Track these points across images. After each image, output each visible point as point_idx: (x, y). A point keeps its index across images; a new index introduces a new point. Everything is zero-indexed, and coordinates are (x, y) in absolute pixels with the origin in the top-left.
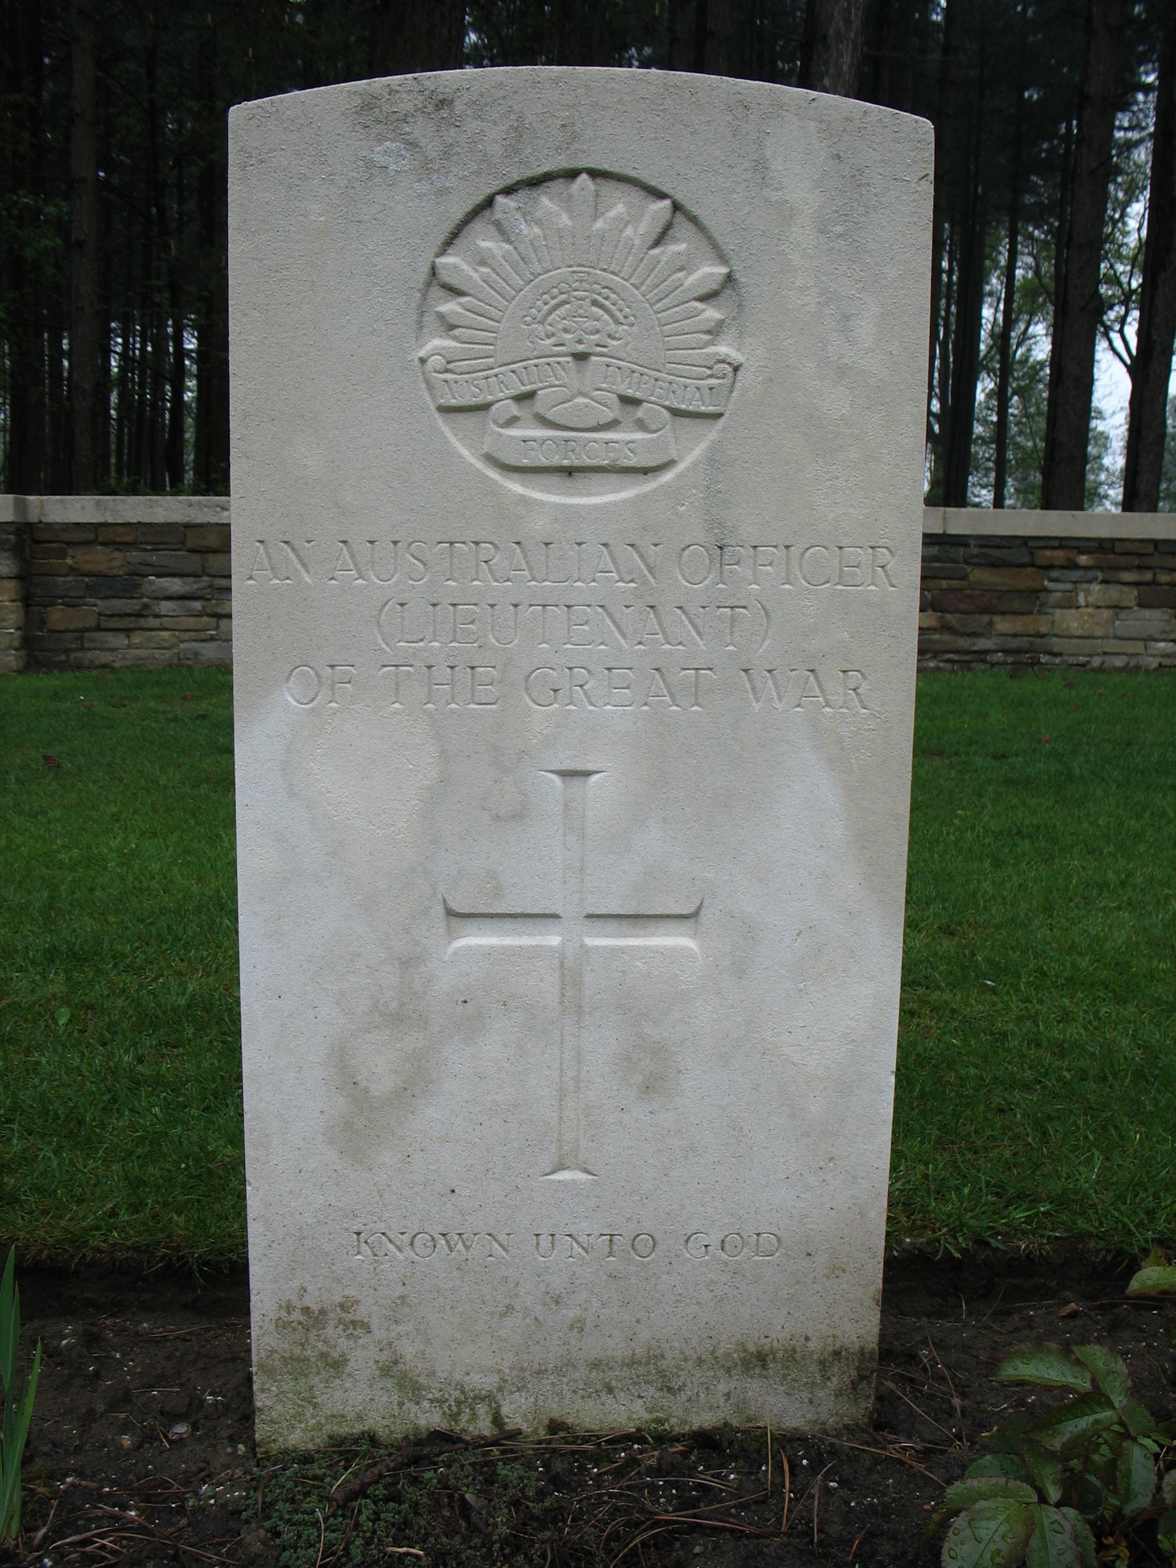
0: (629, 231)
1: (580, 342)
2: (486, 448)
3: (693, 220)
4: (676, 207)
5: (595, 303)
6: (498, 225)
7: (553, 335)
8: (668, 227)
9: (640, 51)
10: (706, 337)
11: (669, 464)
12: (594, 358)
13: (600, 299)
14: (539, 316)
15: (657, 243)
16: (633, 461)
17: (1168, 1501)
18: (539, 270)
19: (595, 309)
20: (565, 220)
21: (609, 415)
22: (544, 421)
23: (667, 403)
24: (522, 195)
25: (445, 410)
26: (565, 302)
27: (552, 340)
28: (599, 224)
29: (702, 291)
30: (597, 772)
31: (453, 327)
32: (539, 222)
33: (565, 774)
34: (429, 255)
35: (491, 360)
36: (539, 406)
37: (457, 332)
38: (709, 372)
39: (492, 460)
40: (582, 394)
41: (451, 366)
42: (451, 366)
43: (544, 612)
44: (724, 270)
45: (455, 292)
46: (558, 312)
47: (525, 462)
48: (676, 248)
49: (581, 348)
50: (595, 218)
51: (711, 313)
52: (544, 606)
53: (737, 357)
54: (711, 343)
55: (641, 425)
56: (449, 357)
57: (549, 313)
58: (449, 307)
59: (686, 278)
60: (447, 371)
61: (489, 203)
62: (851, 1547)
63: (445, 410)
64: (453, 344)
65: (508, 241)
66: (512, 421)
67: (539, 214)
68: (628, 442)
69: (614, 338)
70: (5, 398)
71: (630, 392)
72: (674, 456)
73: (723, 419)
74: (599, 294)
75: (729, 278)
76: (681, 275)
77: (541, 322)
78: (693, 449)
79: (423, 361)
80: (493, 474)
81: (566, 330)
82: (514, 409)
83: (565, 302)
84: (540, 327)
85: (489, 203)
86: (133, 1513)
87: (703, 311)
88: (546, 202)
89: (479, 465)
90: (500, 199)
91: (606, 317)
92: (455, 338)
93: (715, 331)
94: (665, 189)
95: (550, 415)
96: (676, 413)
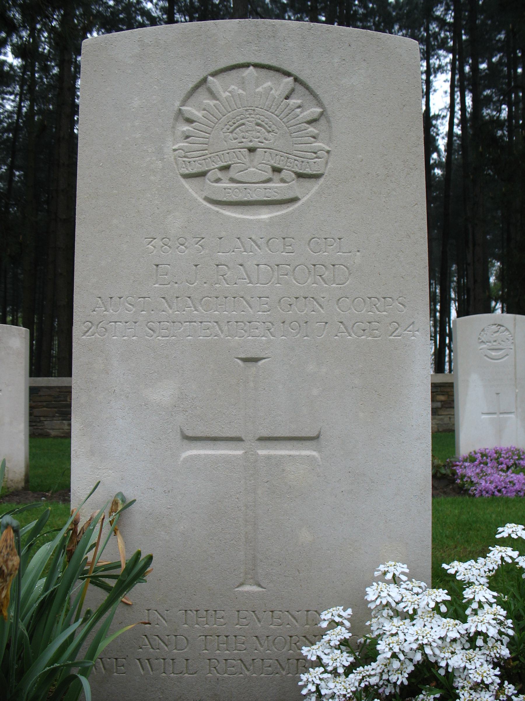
0: (273, 92)
1: (251, 141)
2: (205, 194)
4: (296, 80)
5: (258, 125)
7: (237, 139)
8: (293, 90)
12: (258, 149)
13: (259, 121)
15: (287, 98)
17: (302, 675)
18: (230, 110)
22: (232, 180)
23: (293, 169)
25: (186, 176)
29: (309, 118)
30: (264, 358)
33: (245, 360)
34: (177, 104)
35: (206, 151)
36: (232, 173)
38: (315, 155)
43: (206, 638)
45: (189, 121)
46: (240, 128)
48: (294, 101)
49: (251, 145)
50: (257, 86)
52: (206, 636)
55: (283, 181)
56: (186, 150)
58: (186, 128)
62: (134, 627)
63: (186, 176)
66: (218, 180)
68: (277, 189)
73: (322, 181)
74: (259, 119)
75: (322, 114)
77: (231, 132)
80: (209, 205)
81: (244, 138)
82: (219, 175)
84: (231, 135)
85: (204, 81)
87: (308, 128)
89: (202, 201)
91: (263, 130)
96: (300, 176)
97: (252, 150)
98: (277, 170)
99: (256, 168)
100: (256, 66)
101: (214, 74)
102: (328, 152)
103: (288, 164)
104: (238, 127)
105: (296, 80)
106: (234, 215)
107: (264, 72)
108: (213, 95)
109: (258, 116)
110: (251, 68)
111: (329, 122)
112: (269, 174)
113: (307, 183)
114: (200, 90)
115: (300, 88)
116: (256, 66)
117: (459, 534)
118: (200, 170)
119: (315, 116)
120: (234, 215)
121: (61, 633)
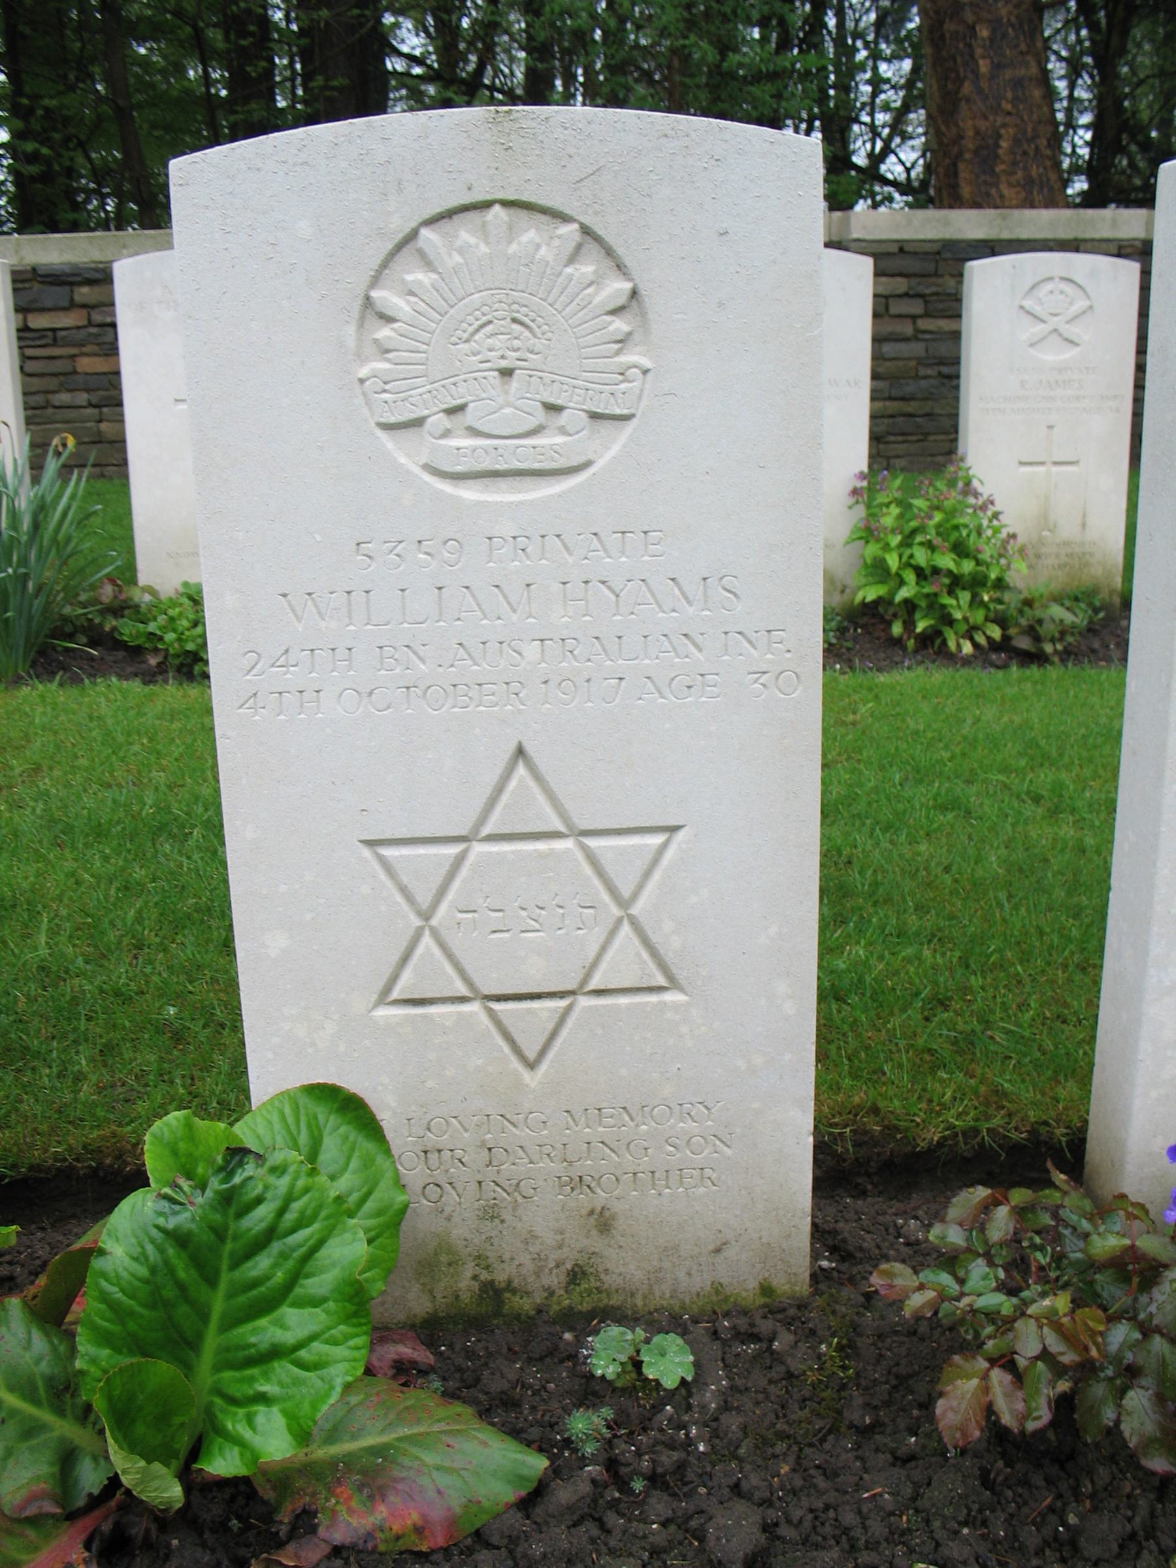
1: (503, 357)
2: (423, 461)
3: (598, 239)
4: (586, 230)
5: (514, 320)
6: (422, 254)
8: (579, 247)
9: (196, 121)
10: (616, 346)
11: (587, 464)
14: (465, 336)
16: (562, 463)
19: (515, 326)
20: (484, 248)
21: (531, 423)
22: (474, 432)
24: (445, 225)
26: (490, 322)
27: (479, 357)
28: (513, 248)
29: (611, 307)
31: (388, 351)
32: (460, 251)
37: (390, 356)
39: (427, 467)
40: (509, 405)
41: (387, 387)
42: (387, 387)
44: (628, 286)
45: (389, 319)
47: (459, 469)
49: (504, 364)
51: (620, 325)
53: (646, 363)
54: (618, 352)
55: (563, 431)
56: (387, 378)
57: (477, 331)
58: (385, 333)
59: (596, 293)
60: (385, 391)
61: (413, 235)
64: (387, 366)
65: (434, 271)
66: (447, 434)
67: (459, 243)
68: (551, 445)
69: (532, 352)
70: (148, 5)
71: (552, 400)
72: (591, 456)
73: (635, 421)
76: (590, 290)
78: (608, 449)
79: (362, 381)
80: (427, 477)
83: (490, 322)
85: (413, 235)
86: (99, 87)
87: (610, 323)
88: (465, 232)
89: (417, 470)
90: (424, 232)
92: (388, 360)
93: (623, 341)
94: (489, 197)
95: (478, 425)
96: (595, 416)
97: (507, 373)
98: (552, 408)
99: (509, 408)
100: (507, 204)
101: (430, 222)
102: (645, 372)
103: (576, 398)
104: (477, 331)
105: (586, 230)
106: (498, 498)
107: (523, 214)
108: (428, 264)
109: (515, 307)
110: (497, 208)
111: (643, 315)
112: (540, 416)
113: (605, 427)
114: (400, 258)
115: (591, 247)
116: (507, 204)
117: (70, 721)
118: (413, 416)
119: (622, 301)
120: (498, 498)
121: (388, 1152)
